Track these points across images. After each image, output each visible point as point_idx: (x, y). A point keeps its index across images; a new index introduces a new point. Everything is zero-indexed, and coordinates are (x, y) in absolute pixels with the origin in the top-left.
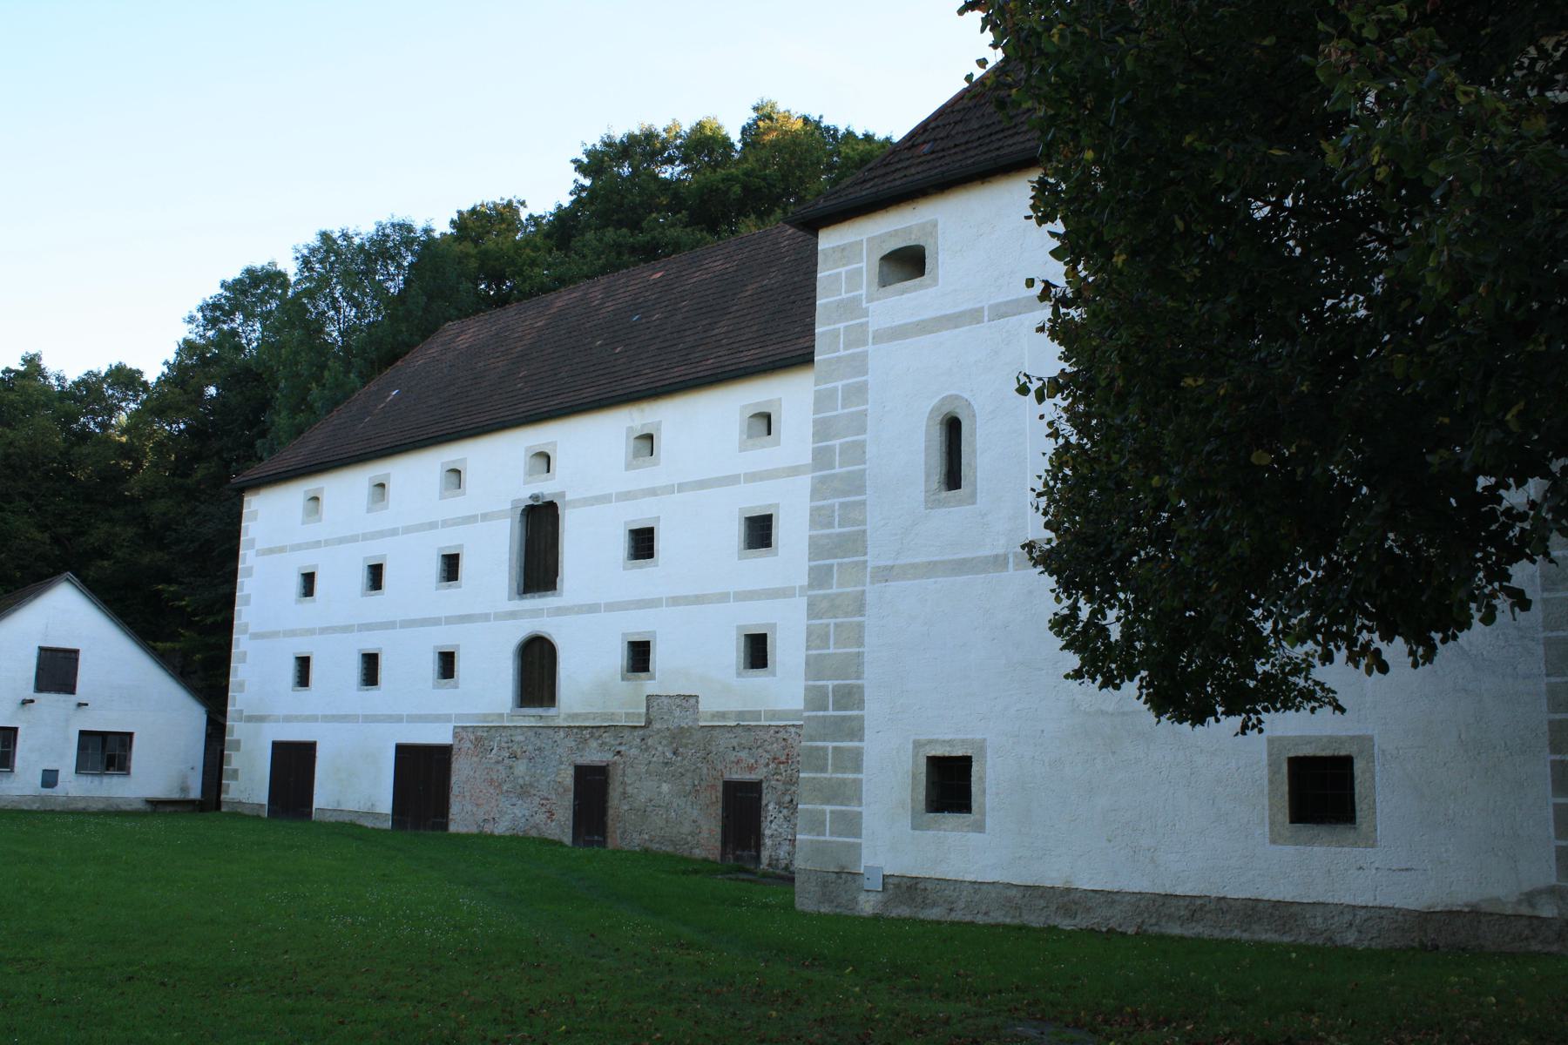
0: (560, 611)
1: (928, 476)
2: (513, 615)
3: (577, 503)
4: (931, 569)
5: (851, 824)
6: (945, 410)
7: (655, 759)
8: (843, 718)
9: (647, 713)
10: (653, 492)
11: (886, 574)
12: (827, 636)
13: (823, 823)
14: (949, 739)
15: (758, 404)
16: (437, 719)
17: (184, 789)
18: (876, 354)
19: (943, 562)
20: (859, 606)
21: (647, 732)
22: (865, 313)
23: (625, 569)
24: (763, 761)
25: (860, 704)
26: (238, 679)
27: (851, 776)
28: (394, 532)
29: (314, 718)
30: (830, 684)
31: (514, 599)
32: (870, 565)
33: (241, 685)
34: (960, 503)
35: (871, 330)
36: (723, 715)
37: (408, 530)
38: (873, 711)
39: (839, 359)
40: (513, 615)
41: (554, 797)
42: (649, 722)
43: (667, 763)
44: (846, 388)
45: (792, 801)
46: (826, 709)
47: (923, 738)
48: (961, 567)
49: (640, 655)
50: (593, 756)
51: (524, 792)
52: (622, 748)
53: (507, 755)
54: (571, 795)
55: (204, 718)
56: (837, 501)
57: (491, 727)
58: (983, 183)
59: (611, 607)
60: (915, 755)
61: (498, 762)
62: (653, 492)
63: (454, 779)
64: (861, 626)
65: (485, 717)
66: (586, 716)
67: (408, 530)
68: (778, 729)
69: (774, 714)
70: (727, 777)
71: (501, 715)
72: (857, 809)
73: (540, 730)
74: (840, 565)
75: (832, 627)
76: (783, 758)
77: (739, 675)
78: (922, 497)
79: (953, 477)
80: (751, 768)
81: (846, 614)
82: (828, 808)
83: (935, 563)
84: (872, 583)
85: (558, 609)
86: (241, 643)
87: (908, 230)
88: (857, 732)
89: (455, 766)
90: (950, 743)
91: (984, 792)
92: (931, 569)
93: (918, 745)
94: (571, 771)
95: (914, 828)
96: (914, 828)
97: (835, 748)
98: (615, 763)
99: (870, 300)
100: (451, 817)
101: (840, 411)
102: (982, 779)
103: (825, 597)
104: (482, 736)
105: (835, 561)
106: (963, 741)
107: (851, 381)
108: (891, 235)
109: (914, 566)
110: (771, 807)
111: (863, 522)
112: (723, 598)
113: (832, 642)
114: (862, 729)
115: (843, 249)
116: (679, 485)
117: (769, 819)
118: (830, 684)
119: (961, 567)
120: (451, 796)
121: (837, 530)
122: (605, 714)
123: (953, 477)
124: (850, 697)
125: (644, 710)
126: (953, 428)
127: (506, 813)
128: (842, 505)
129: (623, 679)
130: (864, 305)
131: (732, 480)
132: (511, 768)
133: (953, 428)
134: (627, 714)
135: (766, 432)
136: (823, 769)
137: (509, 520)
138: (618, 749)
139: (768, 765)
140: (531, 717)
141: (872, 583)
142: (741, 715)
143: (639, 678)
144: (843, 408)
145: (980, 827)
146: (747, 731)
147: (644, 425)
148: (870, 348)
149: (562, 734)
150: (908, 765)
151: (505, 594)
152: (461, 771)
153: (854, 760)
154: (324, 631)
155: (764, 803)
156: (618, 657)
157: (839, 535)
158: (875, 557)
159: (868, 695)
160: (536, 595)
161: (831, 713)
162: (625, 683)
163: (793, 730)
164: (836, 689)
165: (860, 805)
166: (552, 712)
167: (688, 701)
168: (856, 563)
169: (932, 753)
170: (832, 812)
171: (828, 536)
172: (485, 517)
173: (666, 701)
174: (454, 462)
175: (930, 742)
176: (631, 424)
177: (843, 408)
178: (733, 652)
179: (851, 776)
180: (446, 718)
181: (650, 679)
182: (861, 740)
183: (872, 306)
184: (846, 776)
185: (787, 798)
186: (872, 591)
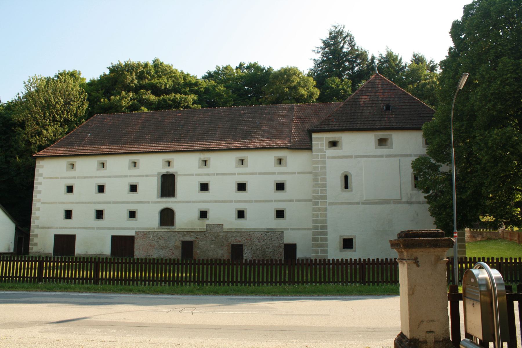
0: (176, 202)
1: (341, 187)
2: (159, 202)
3: (181, 175)
4: (342, 204)
5: (326, 252)
6: (345, 174)
7: (209, 239)
8: (322, 231)
9: (206, 228)
10: (208, 175)
11: (332, 204)
12: (318, 215)
13: (318, 252)
14: (348, 235)
15: (241, 157)
16: (129, 229)
17: (9, 249)
18: (328, 161)
19: (345, 203)
20: (326, 210)
21: (206, 233)
22: (325, 152)
23: (199, 193)
24: (243, 240)
25: (327, 229)
26: (36, 216)
27: (325, 242)
28: (110, 177)
29: (75, 228)
30: (319, 225)
31: (159, 198)
32: (328, 202)
33: (38, 218)
34: (104, 170)
35: (327, 156)
36: (231, 229)
37: (115, 177)
38: (329, 230)
39: (319, 161)
40: (159, 202)
41: (174, 249)
42: (207, 230)
43: (213, 240)
44: (321, 167)
45: (251, 249)
46: (318, 229)
47: (342, 235)
48: (349, 204)
49: (204, 214)
50: (187, 238)
51: (163, 248)
52: (198, 237)
53: (156, 238)
54: (181, 249)
55: (15, 227)
56: (319, 189)
57: (150, 231)
58: (352, 132)
59: (194, 202)
60: (340, 239)
61: (153, 240)
62: (208, 175)
63: (135, 245)
64: (326, 214)
65: (148, 228)
66: (186, 229)
67: (115, 177)
68: (247, 232)
69: (246, 229)
70: (232, 243)
71: (154, 228)
72: (326, 249)
73: (168, 232)
74: (320, 202)
75: (319, 214)
76: (249, 239)
77: (236, 220)
78: (340, 190)
79: (346, 187)
80: (240, 241)
81: (323, 211)
82: (319, 249)
83: (343, 203)
84: (329, 205)
85: (175, 201)
86: (36, 205)
87: (336, 137)
88: (326, 234)
89: (136, 241)
90: (348, 236)
91: (356, 245)
92: (342, 204)
93: (340, 236)
94: (180, 242)
95: (340, 252)
96: (340, 252)
97: (320, 237)
98: (195, 240)
99: (326, 149)
100: (135, 255)
101: (319, 171)
102: (355, 242)
103: (317, 207)
104: (146, 234)
105: (319, 201)
106: (351, 236)
107: (322, 165)
108: (332, 137)
109: (339, 203)
110: (245, 250)
111: (326, 193)
112: (231, 201)
113: (319, 216)
114: (327, 233)
115: (319, 138)
116: (215, 175)
117: (245, 253)
118: (319, 225)
119: (349, 204)
120: (135, 249)
121: (319, 194)
122: (192, 228)
123: (346, 187)
124: (324, 227)
125: (206, 227)
126: (346, 178)
127: (156, 253)
128: (321, 190)
129: (198, 220)
130: (325, 150)
131: (234, 174)
132: (158, 242)
133: (346, 178)
134: (200, 229)
135: (241, 164)
136: (318, 241)
137: (157, 177)
138: (197, 237)
139: (244, 240)
140: (165, 229)
141: (329, 205)
142: (236, 229)
143: (204, 220)
144: (320, 170)
145: (355, 251)
146: (238, 232)
147: (204, 158)
148: (326, 159)
149: (176, 233)
150: (339, 240)
151: (156, 196)
152: (137, 244)
153: (326, 240)
154: (77, 203)
155: (244, 249)
156: (197, 214)
157: (320, 196)
158: (328, 201)
159: (328, 227)
160: (167, 197)
161: (319, 230)
162: (199, 221)
163: (252, 233)
164: (320, 226)
165: (327, 248)
166: (173, 227)
167: (220, 226)
168: (324, 201)
169: (344, 238)
170: (320, 250)
171: (318, 196)
172: (147, 176)
173: (212, 225)
174: (134, 160)
175: (343, 236)
176: (200, 157)
177: (320, 170)
178: (234, 214)
179: (325, 242)
180: (133, 229)
181: (208, 220)
182: (327, 235)
183: (327, 151)
184: (323, 242)
185: (250, 248)
186: (329, 207)
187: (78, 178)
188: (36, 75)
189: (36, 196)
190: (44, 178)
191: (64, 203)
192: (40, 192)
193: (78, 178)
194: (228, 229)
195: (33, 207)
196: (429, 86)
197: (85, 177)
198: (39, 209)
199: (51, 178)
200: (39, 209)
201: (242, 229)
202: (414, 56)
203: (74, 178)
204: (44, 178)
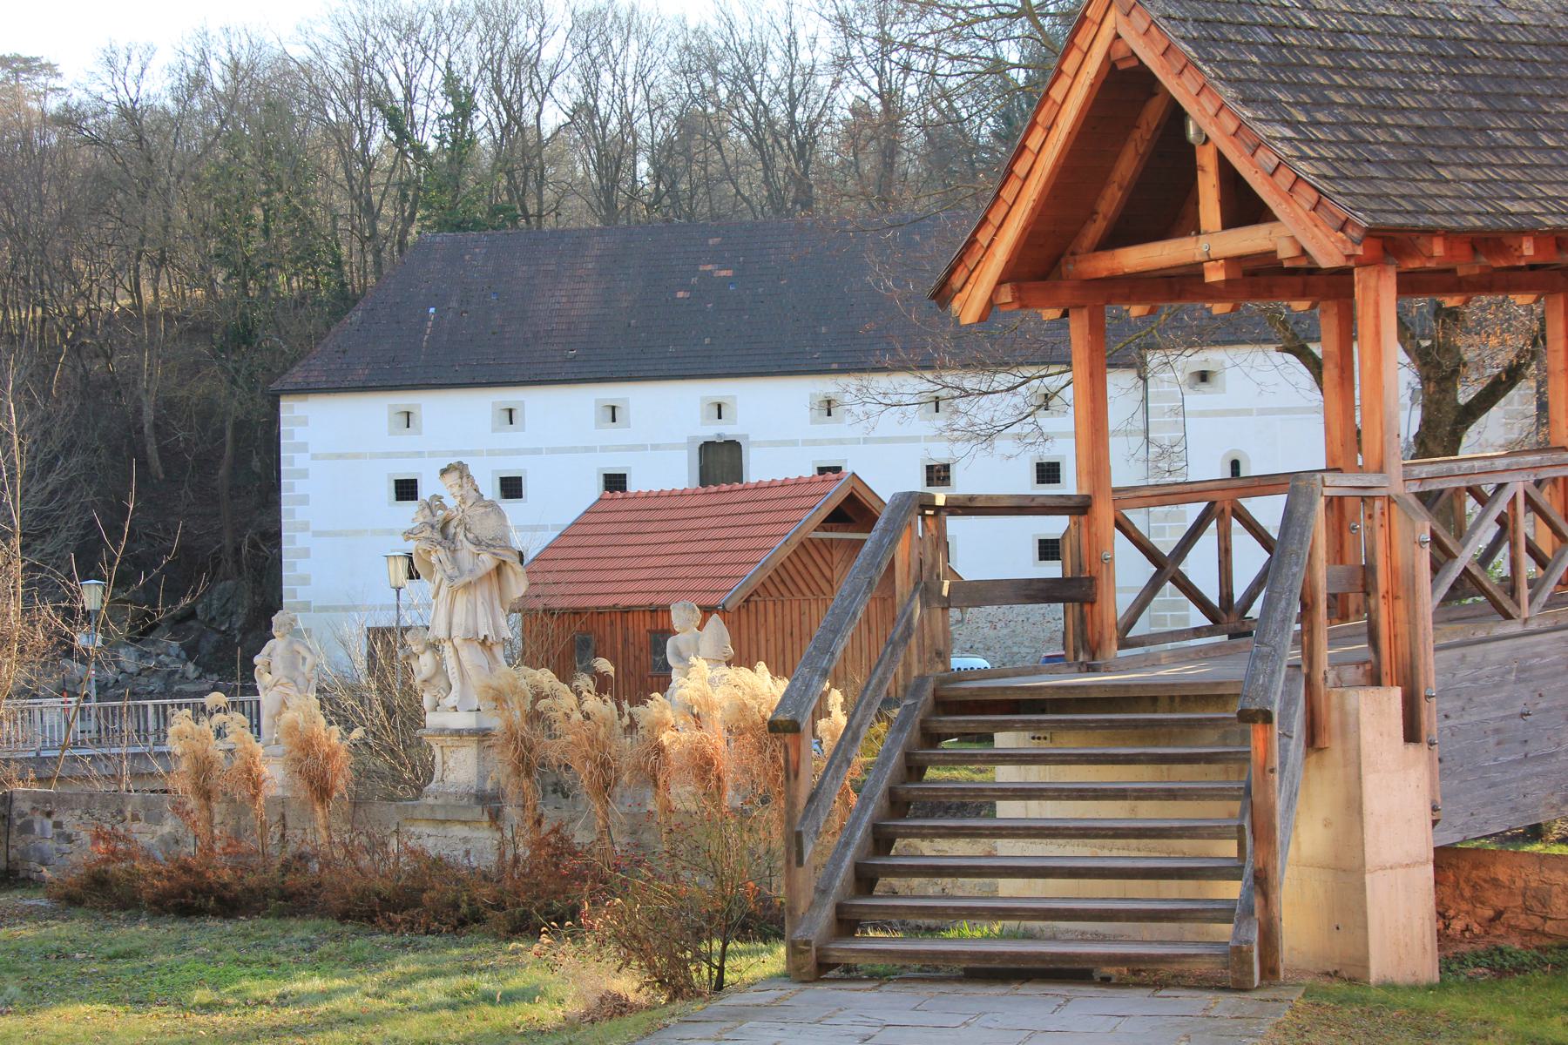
189: (292, 513)
190: (314, 457)
192: (304, 500)
198: (304, 474)
199: (340, 456)
200: (304, 474)
203: (420, 454)
204: (314, 457)
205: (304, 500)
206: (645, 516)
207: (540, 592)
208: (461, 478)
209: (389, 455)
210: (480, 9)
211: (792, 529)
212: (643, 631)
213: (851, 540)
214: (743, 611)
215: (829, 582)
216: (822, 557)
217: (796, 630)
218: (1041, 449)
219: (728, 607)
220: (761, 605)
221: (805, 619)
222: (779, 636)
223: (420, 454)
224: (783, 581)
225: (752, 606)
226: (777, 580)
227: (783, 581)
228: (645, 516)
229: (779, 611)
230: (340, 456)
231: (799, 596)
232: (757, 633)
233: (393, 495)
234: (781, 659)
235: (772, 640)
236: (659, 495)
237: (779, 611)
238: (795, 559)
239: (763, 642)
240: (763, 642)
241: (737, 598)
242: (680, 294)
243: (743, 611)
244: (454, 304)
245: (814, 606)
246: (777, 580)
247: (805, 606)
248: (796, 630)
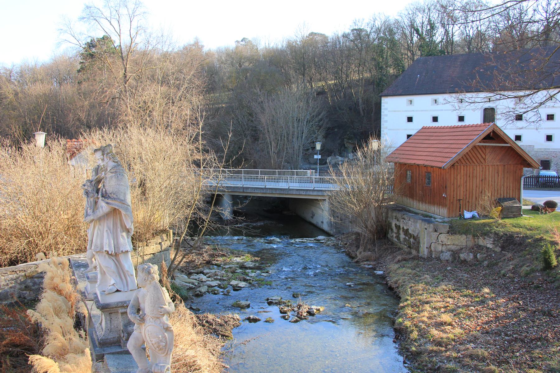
69: (553, 149)
142: (545, 149)
187: (417, 111)
188: (363, 20)
189: (383, 124)
190: (389, 111)
191: (406, 130)
192: (386, 121)
193: (417, 111)
194: (538, 149)
195: (382, 120)
196: (382, 34)
197: (422, 111)
198: (386, 115)
199: (395, 111)
200: (386, 115)
201: (549, 149)
202: (288, 43)
203: (413, 111)
204: (389, 111)
205: (386, 121)
206: (432, 134)
207: (397, 157)
208: (103, 155)
209: (406, 111)
210: (438, 2)
211: (470, 142)
212: (424, 172)
213: (493, 146)
214: (452, 169)
215: (484, 159)
216: (482, 151)
217: (471, 175)
218: (538, 125)
219: (445, 168)
220: (459, 167)
221: (475, 172)
222: (465, 177)
223: (413, 111)
224: (467, 159)
225: (455, 167)
226: (465, 158)
227: (467, 159)
228: (432, 134)
229: (465, 169)
230: (395, 111)
231: (473, 164)
232: (457, 175)
233: (407, 120)
234: (465, 184)
235: (462, 178)
236: (447, 128)
237: (465, 169)
238: (472, 152)
239: (459, 179)
240: (459, 179)
241: (449, 164)
242: (481, 70)
243: (452, 169)
244: (424, 74)
245: (478, 167)
246: (465, 158)
247: (475, 168)
248: (471, 175)
